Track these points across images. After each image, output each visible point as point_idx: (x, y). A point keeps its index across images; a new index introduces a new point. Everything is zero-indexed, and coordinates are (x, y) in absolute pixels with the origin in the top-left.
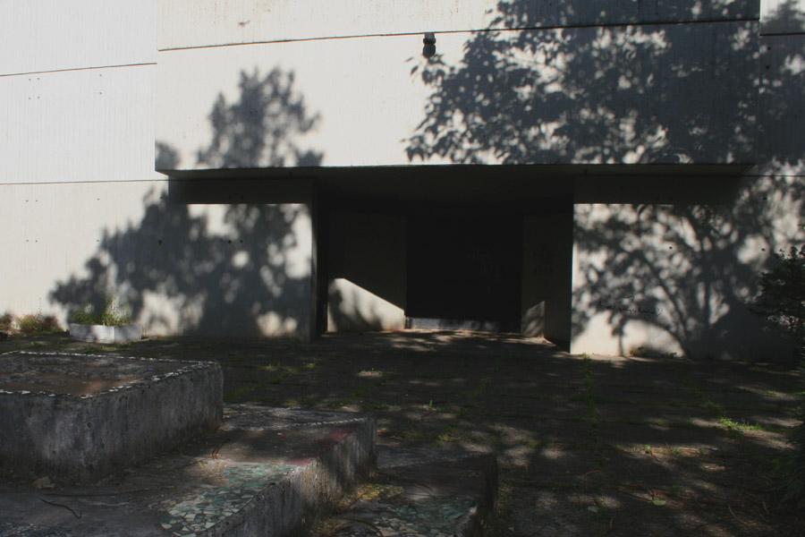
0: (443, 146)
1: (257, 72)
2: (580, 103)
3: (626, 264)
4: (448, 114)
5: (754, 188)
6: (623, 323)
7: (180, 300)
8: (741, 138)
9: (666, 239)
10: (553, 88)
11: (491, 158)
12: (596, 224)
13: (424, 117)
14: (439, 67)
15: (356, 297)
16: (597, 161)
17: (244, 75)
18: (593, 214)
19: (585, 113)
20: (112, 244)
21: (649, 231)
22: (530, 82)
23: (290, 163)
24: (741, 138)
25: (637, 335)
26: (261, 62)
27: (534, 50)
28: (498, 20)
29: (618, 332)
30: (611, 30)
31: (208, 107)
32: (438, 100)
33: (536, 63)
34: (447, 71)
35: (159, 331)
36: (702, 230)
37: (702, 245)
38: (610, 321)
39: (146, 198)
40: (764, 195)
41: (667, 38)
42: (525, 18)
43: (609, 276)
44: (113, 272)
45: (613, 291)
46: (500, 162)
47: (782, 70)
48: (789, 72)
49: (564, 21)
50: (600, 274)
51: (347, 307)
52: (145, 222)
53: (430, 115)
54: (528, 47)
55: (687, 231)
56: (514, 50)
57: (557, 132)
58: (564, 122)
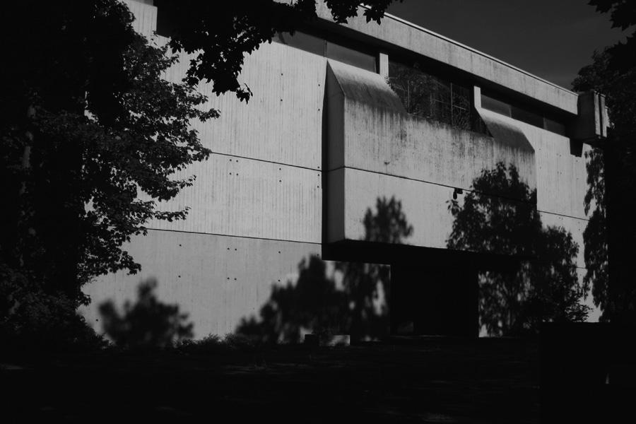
1: (385, 199)
4: (189, 129)
17: (379, 200)
20: (280, 295)
31: (362, 216)
33: (485, 212)
34: (459, 210)
44: (279, 317)
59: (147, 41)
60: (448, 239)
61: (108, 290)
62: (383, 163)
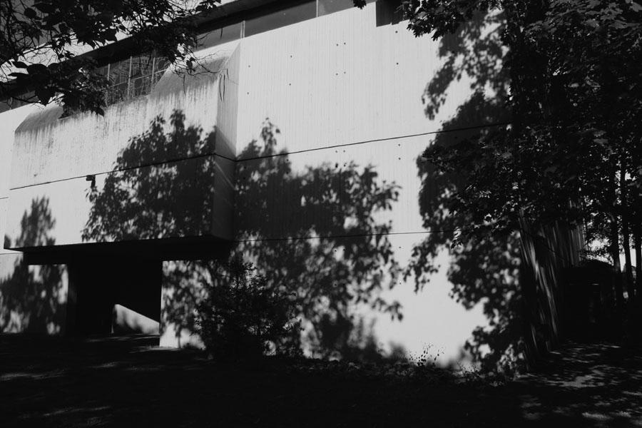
0: (95, 232)
2: (142, 208)
3: (182, 295)
5: (237, 250)
6: (180, 329)
7: (22, 315)
8: (205, 222)
9: (199, 281)
10: (134, 200)
11: (110, 239)
12: (171, 272)
13: (88, 219)
14: (95, 193)
15: (124, 315)
16: (148, 238)
18: (169, 266)
19: (144, 213)
21: (191, 276)
22: (126, 198)
23: (44, 244)
24: (205, 222)
25: (186, 338)
26: (38, 193)
27: (128, 181)
28: (117, 167)
29: (178, 335)
30: (157, 167)
32: (94, 210)
33: (129, 188)
34: (98, 194)
35: (14, 331)
36: (215, 275)
37: (214, 284)
38: (175, 329)
39: (15, 262)
40: (241, 253)
41: (178, 169)
42: (126, 165)
43: (175, 302)
45: (176, 310)
46: (113, 241)
47: (250, 180)
48: (253, 181)
49: (140, 164)
50: (172, 301)
51: (119, 320)
52: (14, 275)
53: (91, 217)
54: (126, 180)
55: (207, 275)
56: (122, 182)
57: (134, 224)
58: (136, 218)
59: (428, 106)
60: (83, 229)
61: (485, 98)
62: (281, 131)
